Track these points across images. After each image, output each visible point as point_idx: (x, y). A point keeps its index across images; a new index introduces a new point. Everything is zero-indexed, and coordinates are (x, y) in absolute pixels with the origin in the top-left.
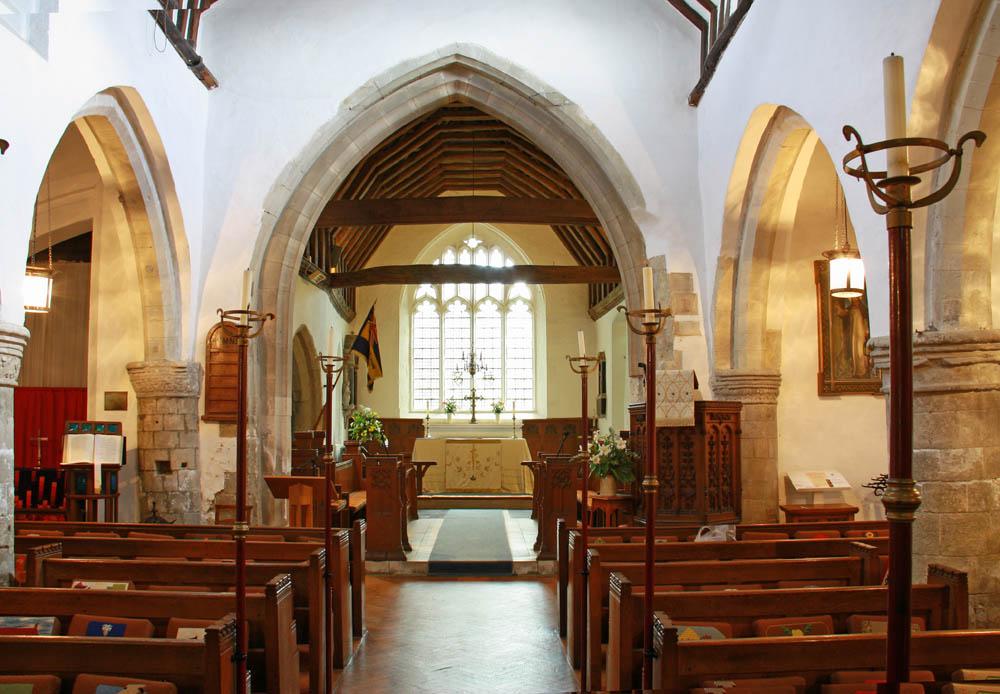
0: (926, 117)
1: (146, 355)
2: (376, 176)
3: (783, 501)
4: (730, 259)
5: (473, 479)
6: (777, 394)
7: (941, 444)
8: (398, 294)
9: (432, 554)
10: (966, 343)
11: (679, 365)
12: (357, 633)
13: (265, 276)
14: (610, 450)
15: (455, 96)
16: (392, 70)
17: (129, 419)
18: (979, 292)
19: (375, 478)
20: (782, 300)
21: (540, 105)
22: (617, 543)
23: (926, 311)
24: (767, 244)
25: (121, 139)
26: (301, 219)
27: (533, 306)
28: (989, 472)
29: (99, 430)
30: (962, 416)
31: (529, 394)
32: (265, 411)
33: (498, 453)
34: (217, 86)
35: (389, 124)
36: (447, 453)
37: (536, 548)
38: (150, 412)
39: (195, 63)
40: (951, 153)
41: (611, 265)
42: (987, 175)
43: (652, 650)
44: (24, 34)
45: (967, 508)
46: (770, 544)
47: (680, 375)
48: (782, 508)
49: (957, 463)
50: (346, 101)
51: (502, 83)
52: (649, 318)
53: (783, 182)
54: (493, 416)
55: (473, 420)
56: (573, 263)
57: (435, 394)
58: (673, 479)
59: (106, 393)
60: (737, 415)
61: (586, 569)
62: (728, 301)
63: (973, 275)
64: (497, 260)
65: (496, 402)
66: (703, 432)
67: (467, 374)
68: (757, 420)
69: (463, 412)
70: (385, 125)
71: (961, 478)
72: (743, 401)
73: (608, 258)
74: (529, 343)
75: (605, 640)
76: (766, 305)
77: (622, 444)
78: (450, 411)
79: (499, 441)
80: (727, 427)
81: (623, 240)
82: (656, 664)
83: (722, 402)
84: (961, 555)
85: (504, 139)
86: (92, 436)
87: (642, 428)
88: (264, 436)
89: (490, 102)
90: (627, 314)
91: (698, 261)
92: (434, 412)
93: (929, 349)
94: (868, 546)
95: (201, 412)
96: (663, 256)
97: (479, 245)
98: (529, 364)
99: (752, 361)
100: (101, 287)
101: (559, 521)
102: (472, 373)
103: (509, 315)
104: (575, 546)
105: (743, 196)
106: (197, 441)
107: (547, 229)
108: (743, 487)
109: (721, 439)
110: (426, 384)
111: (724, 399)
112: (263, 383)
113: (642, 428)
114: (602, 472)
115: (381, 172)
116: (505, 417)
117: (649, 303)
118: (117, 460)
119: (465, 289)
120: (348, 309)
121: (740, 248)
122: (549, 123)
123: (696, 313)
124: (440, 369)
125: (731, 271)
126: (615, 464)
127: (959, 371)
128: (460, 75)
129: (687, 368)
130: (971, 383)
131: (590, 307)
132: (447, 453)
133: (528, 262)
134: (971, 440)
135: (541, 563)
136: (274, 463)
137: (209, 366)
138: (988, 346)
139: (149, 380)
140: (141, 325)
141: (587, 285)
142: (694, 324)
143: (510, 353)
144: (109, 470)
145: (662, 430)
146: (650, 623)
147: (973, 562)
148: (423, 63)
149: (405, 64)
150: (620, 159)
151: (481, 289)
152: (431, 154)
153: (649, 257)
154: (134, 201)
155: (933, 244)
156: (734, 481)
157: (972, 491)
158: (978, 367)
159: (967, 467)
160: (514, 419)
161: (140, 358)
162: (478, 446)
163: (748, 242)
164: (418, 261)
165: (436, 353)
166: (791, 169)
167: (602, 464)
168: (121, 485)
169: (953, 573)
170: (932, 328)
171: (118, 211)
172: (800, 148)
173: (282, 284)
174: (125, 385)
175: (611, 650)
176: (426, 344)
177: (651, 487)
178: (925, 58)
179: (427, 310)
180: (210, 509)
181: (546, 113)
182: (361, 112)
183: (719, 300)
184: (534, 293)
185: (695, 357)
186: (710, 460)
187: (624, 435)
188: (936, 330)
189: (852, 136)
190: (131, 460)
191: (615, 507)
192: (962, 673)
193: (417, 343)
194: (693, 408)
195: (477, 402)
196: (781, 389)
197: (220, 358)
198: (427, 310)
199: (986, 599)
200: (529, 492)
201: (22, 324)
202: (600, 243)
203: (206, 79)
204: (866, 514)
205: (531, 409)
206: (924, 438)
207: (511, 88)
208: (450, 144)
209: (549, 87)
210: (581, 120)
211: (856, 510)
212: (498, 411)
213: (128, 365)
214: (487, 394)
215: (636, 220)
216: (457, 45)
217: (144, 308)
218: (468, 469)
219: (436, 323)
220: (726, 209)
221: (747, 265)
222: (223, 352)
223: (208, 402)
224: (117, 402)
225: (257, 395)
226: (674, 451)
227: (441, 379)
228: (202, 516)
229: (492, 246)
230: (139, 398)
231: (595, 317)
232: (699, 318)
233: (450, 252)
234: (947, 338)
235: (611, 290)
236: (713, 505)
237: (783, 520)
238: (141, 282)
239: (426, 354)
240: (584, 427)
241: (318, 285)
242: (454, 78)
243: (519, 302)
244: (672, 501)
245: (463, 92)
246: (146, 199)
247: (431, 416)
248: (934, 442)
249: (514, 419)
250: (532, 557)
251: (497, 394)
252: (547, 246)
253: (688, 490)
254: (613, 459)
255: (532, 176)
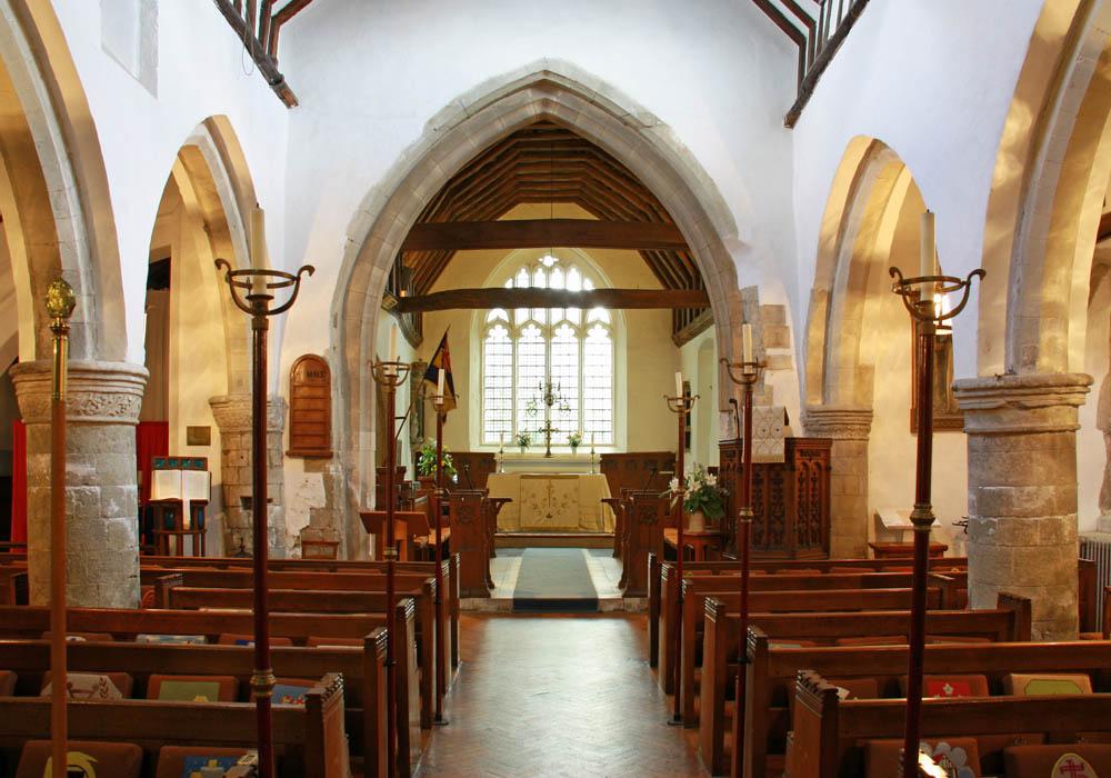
0: (1011, 168)
1: (230, 389)
2: (448, 190)
3: (872, 538)
4: (823, 291)
5: (549, 516)
6: (868, 431)
7: (1016, 482)
8: (469, 317)
9: (515, 592)
10: (1043, 387)
11: (769, 401)
12: (455, 664)
13: (349, 306)
14: (699, 487)
15: (544, 114)
16: (480, 88)
17: (213, 452)
18: (1056, 338)
19: (459, 514)
20: (875, 334)
21: (630, 126)
22: (705, 575)
23: (1007, 356)
24: (861, 277)
25: (210, 167)
26: (386, 246)
27: (613, 331)
28: (1060, 508)
29: (185, 465)
30: (1036, 455)
31: (608, 426)
32: (349, 446)
33: (576, 490)
34: (297, 105)
35: (475, 146)
36: (521, 489)
37: (621, 586)
38: (234, 448)
39: (277, 82)
40: (963, 283)
41: (698, 288)
42: (1066, 225)
43: (746, 657)
44: (135, 71)
45: (1038, 542)
46: (857, 577)
47: (770, 411)
48: (872, 546)
49: (1031, 500)
50: (431, 122)
51: (592, 102)
52: (748, 370)
53: (879, 213)
54: (569, 450)
55: (548, 454)
56: (657, 285)
57: (508, 427)
58: (762, 515)
59: (189, 428)
60: (828, 452)
61: (680, 597)
62: (821, 335)
63: (1051, 322)
64: (574, 281)
65: (572, 435)
66: (793, 469)
67: (542, 405)
68: (848, 457)
69: (538, 446)
70: (472, 145)
71: (1033, 513)
72: (833, 437)
73: (693, 278)
74: (608, 370)
75: (698, 662)
76: (859, 339)
77: (712, 480)
78: (524, 443)
79: (576, 477)
80: (818, 464)
81: (715, 269)
82: (749, 669)
83: (814, 439)
84: (1032, 585)
85: (586, 149)
86: (179, 471)
87: (731, 466)
88: (349, 471)
89: (579, 123)
90: (728, 366)
91: (791, 292)
92: (507, 445)
93: (1007, 392)
94: (947, 578)
95: (286, 447)
96: (757, 287)
97: (555, 263)
98: (608, 393)
99: (845, 396)
100: (182, 319)
101: (650, 555)
102: (550, 404)
103: (587, 340)
104: (668, 578)
105: (838, 226)
106: (282, 477)
107: (635, 254)
108: (832, 524)
109: (811, 476)
110: (497, 415)
111: (814, 435)
112: (348, 418)
113: (731, 466)
114: (692, 507)
115: (452, 187)
116: (582, 451)
117: (748, 358)
118: (204, 496)
119: (540, 314)
120: (415, 337)
121: (833, 280)
122: (640, 144)
123: (788, 347)
124: (513, 399)
125: (824, 304)
126: (705, 500)
127: (1034, 413)
128: (547, 92)
129: (778, 404)
130: (1045, 425)
131: (674, 333)
132: (521, 489)
133: (609, 285)
134: (1044, 478)
135: (628, 600)
136: (358, 498)
137: (293, 400)
138: (1063, 390)
139: (234, 415)
140: (224, 360)
141: (670, 311)
142: (786, 358)
143: (588, 382)
144: (197, 506)
145: (754, 465)
146: (745, 635)
147: (1042, 590)
148: (510, 80)
149: (491, 81)
150: (713, 185)
151: (557, 314)
152: (508, 164)
153: (741, 288)
154: (219, 231)
155: (1015, 291)
156: (823, 517)
157: (1044, 526)
158: (1053, 409)
159: (1040, 503)
160: (593, 453)
161: (223, 391)
162: (554, 482)
163: (842, 273)
164: (487, 285)
165: (508, 382)
166: (887, 200)
167: (692, 500)
168: (207, 520)
169: (1018, 600)
170: (1011, 372)
171: (202, 240)
172: (897, 179)
173: (365, 315)
174: (207, 420)
175: (705, 674)
176: (498, 371)
177: (747, 517)
178: (1010, 111)
179: (499, 334)
180: (295, 546)
181: (637, 134)
182: (447, 133)
183: (811, 334)
184: (614, 319)
185: (786, 392)
186: (799, 496)
187: (712, 470)
188: (1015, 374)
189: (896, 274)
190: (217, 494)
191: (704, 542)
192: (1010, 678)
193: (488, 371)
194: (783, 444)
195: (553, 435)
196: (873, 424)
197: (303, 392)
198: (499, 334)
199: (1052, 625)
200: (609, 530)
201: (143, 363)
202: (686, 264)
203: (287, 97)
204: (956, 549)
205: (610, 442)
206: (1001, 476)
207: (601, 107)
208: (527, 154)
209: (641, 107)
210: (672, 142)
211: (945, 548)
212: (575, 445)
213: (213, 398)
214: (563, 426)
215: (728, 249)
216: (545, 61)
217: (227, 341)
218: (544, 505)
219: (509, 349)
220: (821, 239)
221: (840, 298)
222: (308, 386)
223: (293, 436)
224: (198, 436)
225: (342, 430)
226: (764, 487)
227: (514, 411)
228: (287, 552)
229: (569, 264)
230: (222, 433)
231: (679, 343)
232: (791, 351)
233: (523, 270)
234: (1024, 382)
235: (697, 315)
236: (801, 542)
237: (871, 555)
238: (225, 314)
239: (498, 382)
240: (671, 463)
241: (388, 311)
242: (543, 96)
243: (598, 326)
244: (760, 537)
245: (553, 111)
246: (231, 228)
247: (506, 450)
248: (1010, 480)
249: (593, 453)
250: (618, 594)
251: (574, 426)
252: (633, 270)
253: (777, 526)
254: (703, 495)
255: (614, 189)
